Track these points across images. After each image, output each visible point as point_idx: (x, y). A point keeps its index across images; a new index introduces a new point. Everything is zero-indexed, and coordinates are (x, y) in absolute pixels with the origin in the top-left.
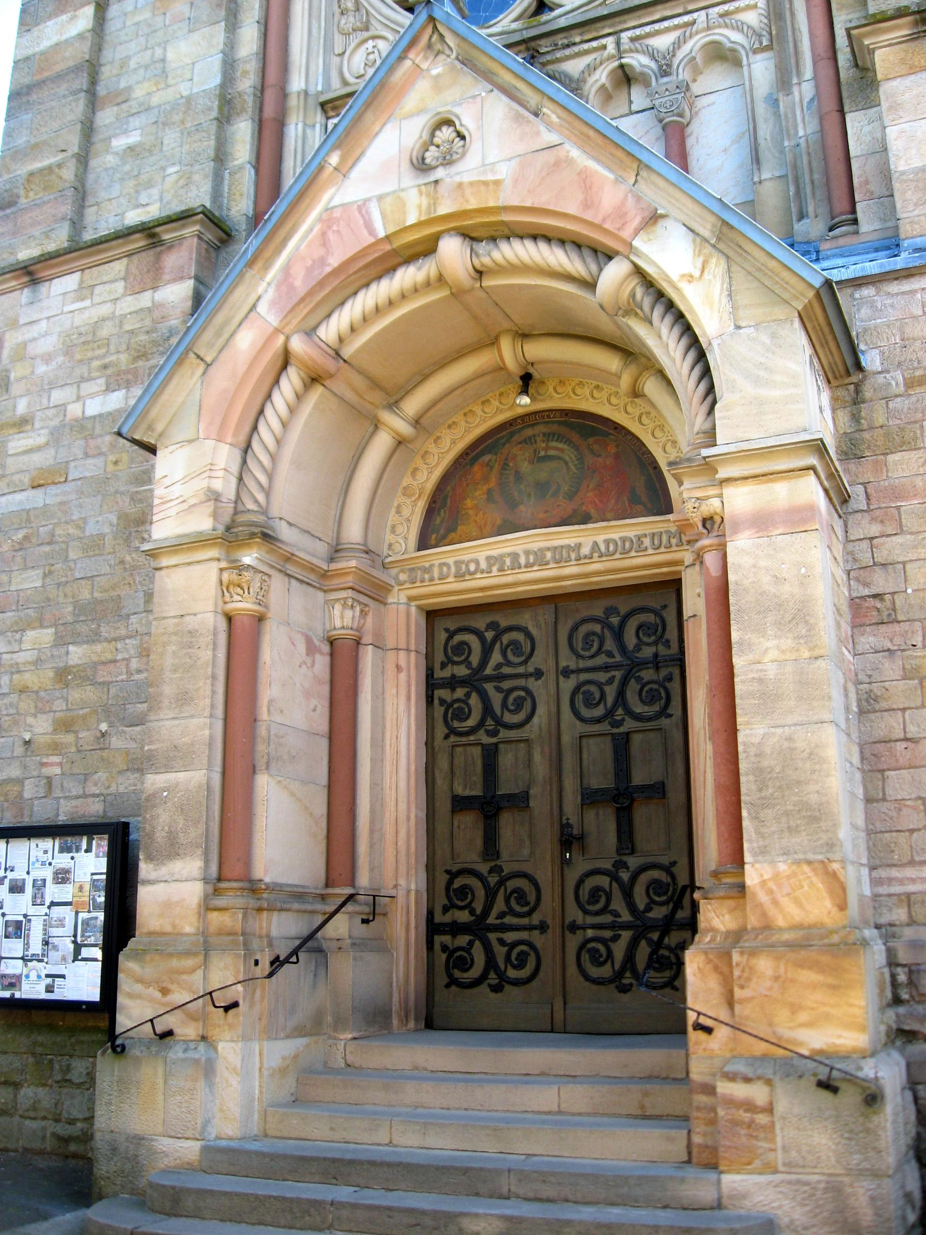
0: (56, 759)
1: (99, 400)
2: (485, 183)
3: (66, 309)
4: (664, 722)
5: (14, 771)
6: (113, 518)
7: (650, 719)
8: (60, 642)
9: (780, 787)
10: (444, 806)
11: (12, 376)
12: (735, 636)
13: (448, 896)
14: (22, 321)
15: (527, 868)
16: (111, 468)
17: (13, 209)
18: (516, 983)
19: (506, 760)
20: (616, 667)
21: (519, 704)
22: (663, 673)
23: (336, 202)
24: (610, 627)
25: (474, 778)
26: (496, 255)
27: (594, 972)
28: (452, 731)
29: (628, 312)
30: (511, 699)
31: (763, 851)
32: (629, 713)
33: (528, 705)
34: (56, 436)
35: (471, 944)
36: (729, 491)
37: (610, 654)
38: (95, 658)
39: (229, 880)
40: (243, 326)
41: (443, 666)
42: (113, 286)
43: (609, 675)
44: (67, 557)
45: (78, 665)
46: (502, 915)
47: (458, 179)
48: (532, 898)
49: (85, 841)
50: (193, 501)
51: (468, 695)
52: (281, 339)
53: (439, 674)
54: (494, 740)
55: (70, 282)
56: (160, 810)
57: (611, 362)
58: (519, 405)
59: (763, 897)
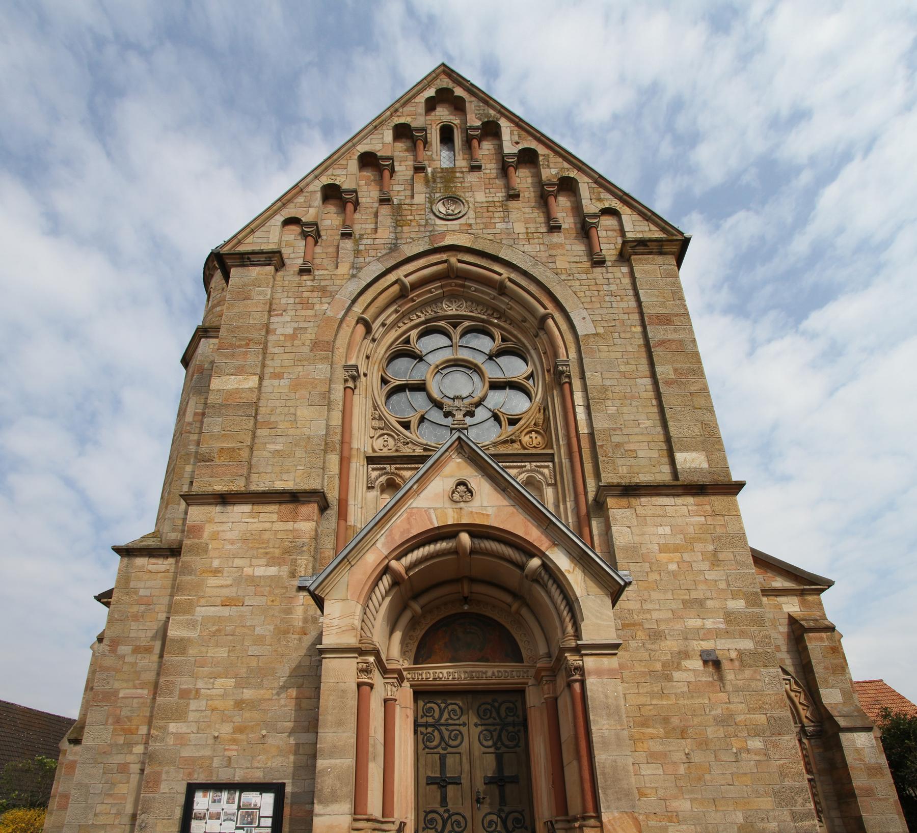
0: (235, 747)
3: (243, 520)
6: (271, 628)
8: (238, 686)
9: (613, 781)
10: (423, 781)
11: (210, 547)
13: (425, 822)
15: (461, 811)
16: (269, 603)
17: (211, 463)
20: (498, 725)
21: (456, 736)
23: (414, 505)
25: (436, 769)
28: (426, 747)
31: (608, 807)
32: (503, 744)
34: (238, 582)
36: (586, 659)
37: (494, 719)
39: (361, 815)
41: (422, 717)
42: (271, 515)
43: (494, 727)
44: (243, 644)
45: (248, 699)
47: (470, 509)
48: (463, 824)
50: (345, 628)
51: (433, 731)
54: (445, 752)
56: (326, 778)
58: (752, 638)
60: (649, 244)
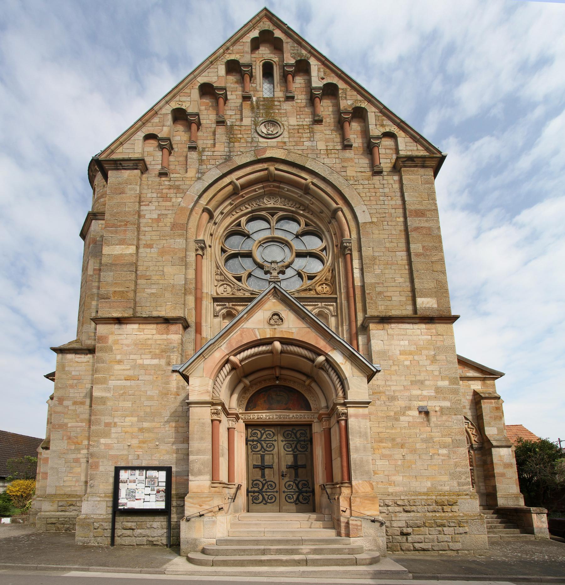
2: (289, 332)
3: (134, 333)
4: (306, 452)
5: (125, 452)
6: (157, 392)
10: (251, 467)
11: (114, 348)
16: (155, 379)
18: (270, 503)
19: (267, 458)
22: (306, 443)
23: (244, 327)
24: (293, 432)
27: (289, 501)
28: (253, 451)
32: (298, 450)
33: (272, 447)
36: (349, 409)
37: (293, 438)
38: (153, 426)
40: (217, 350)
47: (281, 329)
51: (257, 444)
53: (249, 438)
55: (136, 326)
59: (356, 487)
60: (415, 159)
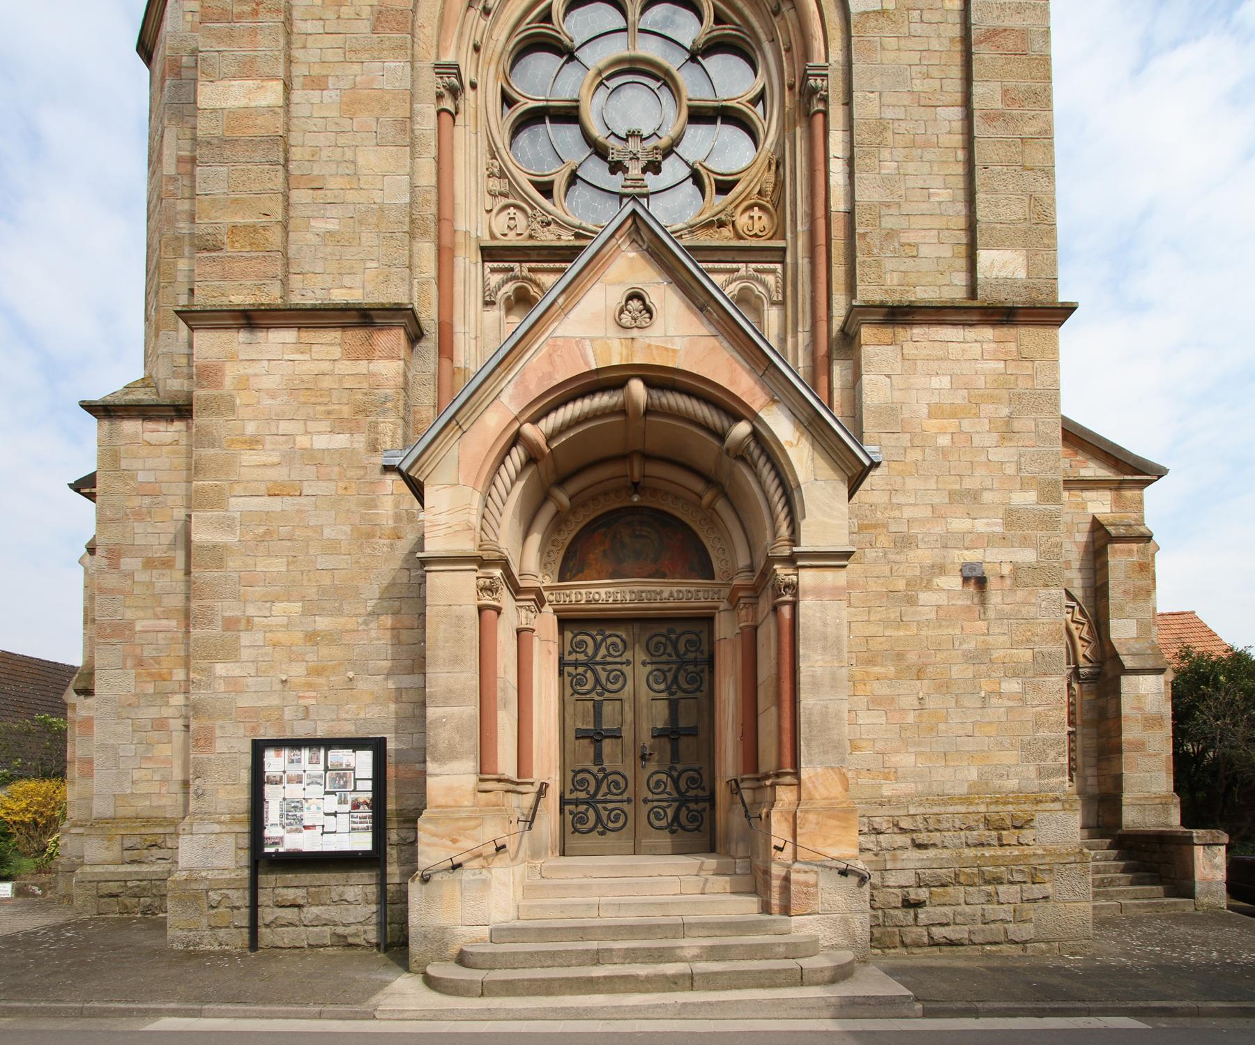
1: (325, 438)
2: (666, 349)
4: (698, 694)
5: (275, 701)
6: (347, 529)
7: (691, 692)
8: (306, 612)
10: (571, 735)
12: (802, 651)
14: (241, 357)
15: (620, 770)
16: (341, 492)
19: (607, 709)
21: (616, 679)
24: (670, 640)
26: (664, 400)
27: (657, 823)
28: (576, 692)
29: (742, 458)
30: (611, 676)
31: (810, 762)
32: (679, 687)
35: (587, 810)
36: (802, 572)
37: (670, 655)
38: (340, 628)
40: (489, 409)
41: (570, 653)
42: (330, 348)
43: (669, 666)
46: (605, 794)
47: (647, 341)
49: (322, 751)
51: (585, 672)
52: (517, 425)
56: (441, 730)
57: (699, 486)
59: (809, 785)
